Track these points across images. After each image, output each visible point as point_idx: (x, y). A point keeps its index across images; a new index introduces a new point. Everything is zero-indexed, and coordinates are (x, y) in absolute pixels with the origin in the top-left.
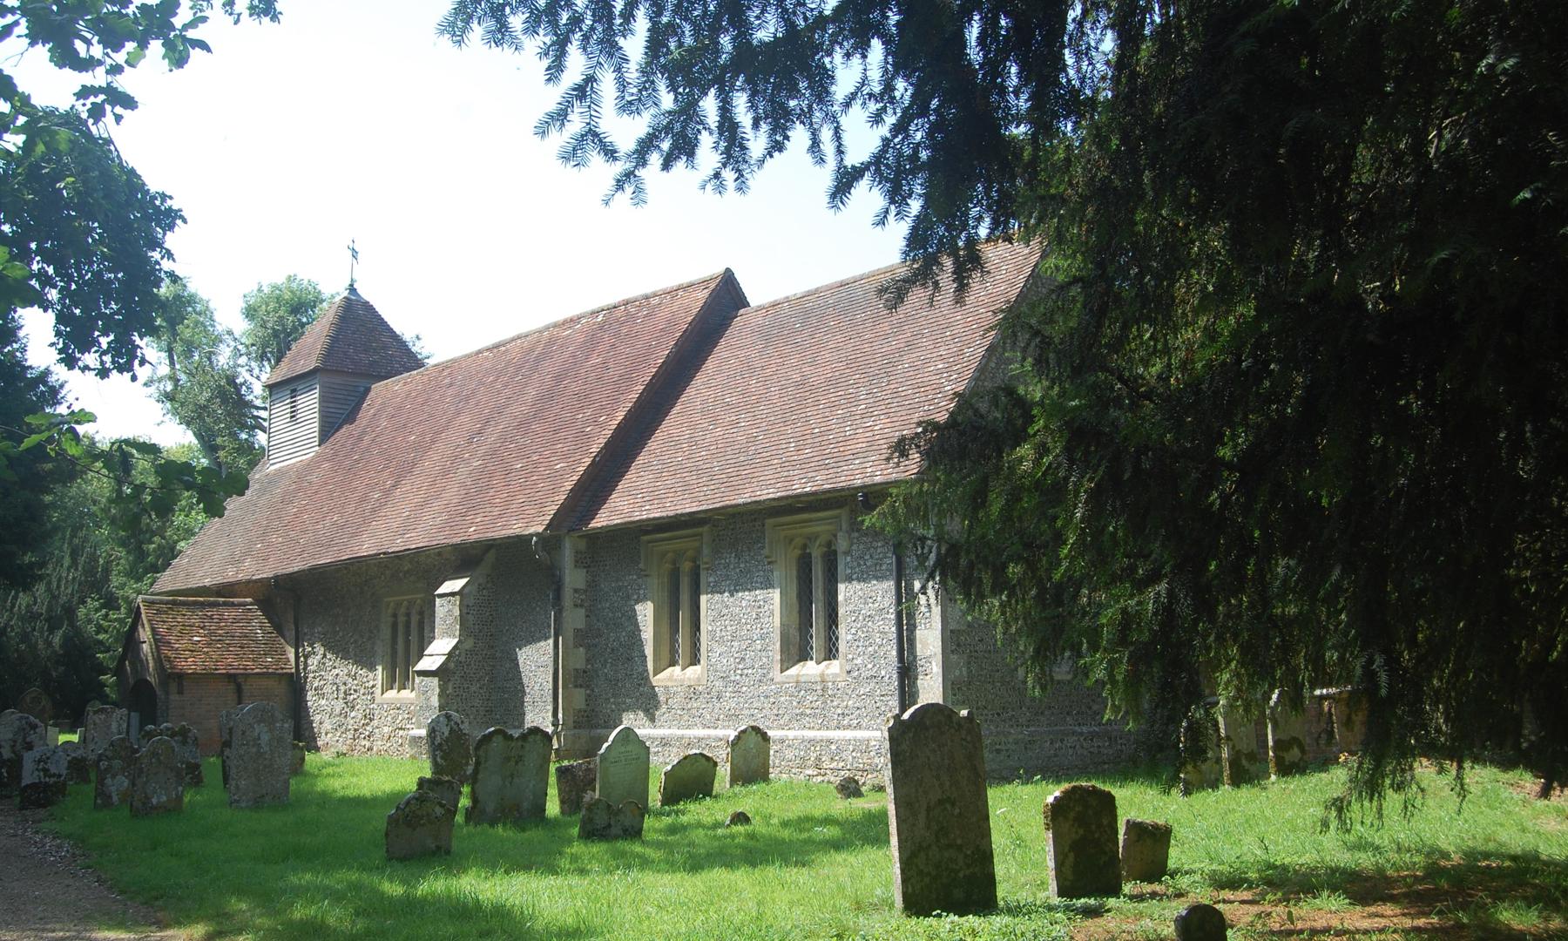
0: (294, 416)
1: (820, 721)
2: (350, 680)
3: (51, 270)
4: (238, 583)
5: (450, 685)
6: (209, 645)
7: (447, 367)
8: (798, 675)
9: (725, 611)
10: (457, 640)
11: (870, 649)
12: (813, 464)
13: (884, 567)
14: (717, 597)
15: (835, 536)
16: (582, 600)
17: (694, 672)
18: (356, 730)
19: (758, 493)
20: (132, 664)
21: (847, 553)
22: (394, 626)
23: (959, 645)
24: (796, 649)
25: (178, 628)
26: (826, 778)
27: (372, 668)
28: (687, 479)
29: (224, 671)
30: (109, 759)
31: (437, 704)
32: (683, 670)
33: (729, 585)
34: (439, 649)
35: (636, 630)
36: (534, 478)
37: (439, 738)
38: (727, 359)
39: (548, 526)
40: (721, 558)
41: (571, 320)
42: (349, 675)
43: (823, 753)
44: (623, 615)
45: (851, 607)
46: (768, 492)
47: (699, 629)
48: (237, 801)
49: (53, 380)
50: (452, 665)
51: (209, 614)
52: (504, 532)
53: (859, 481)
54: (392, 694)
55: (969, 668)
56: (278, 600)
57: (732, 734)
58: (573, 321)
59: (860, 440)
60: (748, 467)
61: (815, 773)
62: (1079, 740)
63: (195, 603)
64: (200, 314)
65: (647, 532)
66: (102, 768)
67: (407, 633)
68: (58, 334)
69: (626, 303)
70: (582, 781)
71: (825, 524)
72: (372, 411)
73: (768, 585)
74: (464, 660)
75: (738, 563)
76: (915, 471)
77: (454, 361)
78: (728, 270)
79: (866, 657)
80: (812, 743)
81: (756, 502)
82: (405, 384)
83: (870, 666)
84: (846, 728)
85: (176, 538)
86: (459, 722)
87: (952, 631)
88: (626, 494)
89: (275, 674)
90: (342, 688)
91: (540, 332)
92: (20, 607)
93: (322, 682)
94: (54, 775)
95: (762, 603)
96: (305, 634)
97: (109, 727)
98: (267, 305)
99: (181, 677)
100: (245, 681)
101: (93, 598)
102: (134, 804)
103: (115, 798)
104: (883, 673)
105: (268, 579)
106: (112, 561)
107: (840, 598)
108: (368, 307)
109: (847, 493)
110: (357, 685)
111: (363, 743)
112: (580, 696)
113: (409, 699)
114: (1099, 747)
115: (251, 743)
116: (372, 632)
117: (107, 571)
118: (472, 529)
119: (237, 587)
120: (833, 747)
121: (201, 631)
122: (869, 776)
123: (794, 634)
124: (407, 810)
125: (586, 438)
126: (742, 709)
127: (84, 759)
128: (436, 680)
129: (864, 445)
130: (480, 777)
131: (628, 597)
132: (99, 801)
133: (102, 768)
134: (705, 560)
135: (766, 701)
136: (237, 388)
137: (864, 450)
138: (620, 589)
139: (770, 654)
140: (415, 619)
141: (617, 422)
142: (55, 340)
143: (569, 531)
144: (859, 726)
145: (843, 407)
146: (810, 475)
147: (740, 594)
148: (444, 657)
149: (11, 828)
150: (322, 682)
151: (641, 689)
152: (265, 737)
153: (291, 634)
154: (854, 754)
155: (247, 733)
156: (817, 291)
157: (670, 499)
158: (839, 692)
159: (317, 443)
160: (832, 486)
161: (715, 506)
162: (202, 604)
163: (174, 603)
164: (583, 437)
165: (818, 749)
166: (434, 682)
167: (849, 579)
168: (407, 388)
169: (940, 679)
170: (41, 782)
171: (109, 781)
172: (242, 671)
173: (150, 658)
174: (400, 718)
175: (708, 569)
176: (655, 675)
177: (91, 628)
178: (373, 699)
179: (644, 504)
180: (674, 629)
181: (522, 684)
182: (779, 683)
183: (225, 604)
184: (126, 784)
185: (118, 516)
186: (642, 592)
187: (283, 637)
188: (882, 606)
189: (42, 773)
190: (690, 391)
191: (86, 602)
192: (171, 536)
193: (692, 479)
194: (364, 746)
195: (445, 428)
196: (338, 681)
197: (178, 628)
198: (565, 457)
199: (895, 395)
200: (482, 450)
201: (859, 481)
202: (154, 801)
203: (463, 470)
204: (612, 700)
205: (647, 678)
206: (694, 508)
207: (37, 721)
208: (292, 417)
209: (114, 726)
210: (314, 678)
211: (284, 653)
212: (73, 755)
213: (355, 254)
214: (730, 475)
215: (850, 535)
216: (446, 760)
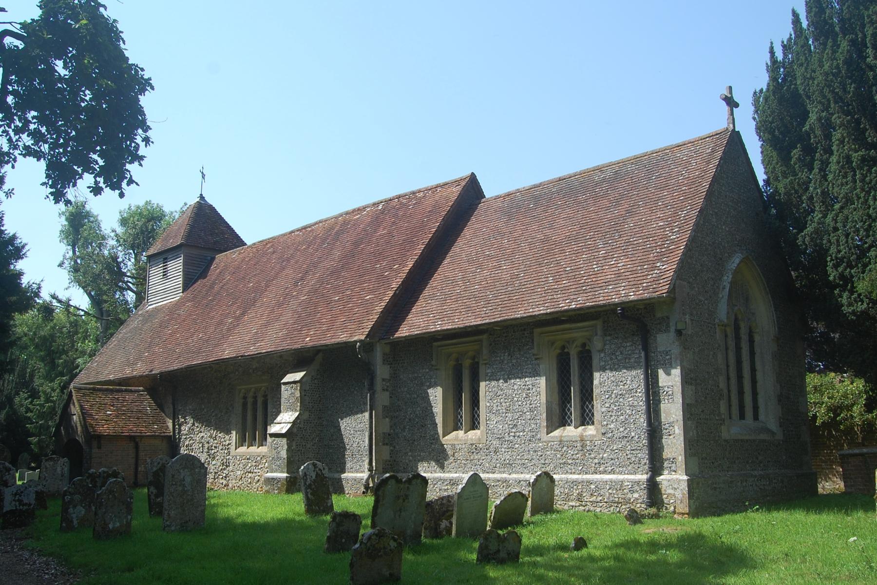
0: (166, 275)
1: (581, 468)
2: (212, 440)
3: (44, 130)
4: (134, 377)
5: (294, 444)
6: (117, 417)
8: (561, 436)
9: (500, 393)
10: (297, 414)
11: (622, 417)
12: (572, 290)
14: (493, 383)
15: (589, 340)
16: (388, 387)
18: (215, 473)
19: (531, 310)
20: (66, 429)
22: (245, 405)
23: (691, 415)
25: (97, 406)
27: (228, 432)
28: (467, 303)
29: (127, 434)
30: (71, 494)
31: (285, 456)
32: (465, 433)
35: (429, 406)
36: (351, 305)
37: (309, 480)
38: (480, 229)
39: (368, 336)
41: (359, 209)
42: (211, 437)
43: (584, 490)
46: (539, 309)
47: (256, 421)
48: (168, 526)
49: (18, 242)
50: (295, 430)
51: (117, 397)
52: (333, 340)
53: (617, 300)
54: (243, 449)
55: (697, 431)
56: (161, 388)
57: (532, 478)
58: (359, 210)
60: (517, 294)
61: (577, 504)
63: (107, 390)
64: (92, 222)
65: (437, 340)
66: (66, 501)
67: (255, 410)
68: (48, 176)
69: (399, 197)
70: (438, 513)
71: (587, 331)
72: (218, 271)
73: (535, 374)
76: (666, 291)
78: (473, 174)
79: (618, 423)
80: (575, 483)
81: (531, 316)
82: (240, 254)
83: (621, 429)
84: (605, 472)
85: (75, 356)
86: (322, 469)
87: (688, 404)
90: (206, 445)
91: (336, 217)
93: (191, 442)
94: (26, 504)
95: (530, 387)
96: (179, 410)
98: (134, 217)
99: (99, 437)
100: (141, 441)
101: (24, 392)
103: (75, 522)
104: (633, 434)
106: (35, 370)
107: (596, 382)
109: (608, 308)
110: (217, 443)
111: (221, 481)
112: (386, 450)
115: (179, 483)
116: (228, 409)
117: (32, 376)
118: (308, 339)
119: (130, 381)
120: (593, 487)
121: (112, 408)
122: (623, 507)
123: (556, 408)
124: (368, 544)
126: (515, 460)
128: (284, 440)
130: (379, 511)
131: (422, 384)
132: (64, 525)
133: (66, 501)
136: (118, 264)
137: (614, 279)
139: (538, 421)
140: (260, 400)
141: (409, 268)
143: (380, 339)
144: (613, 472)
145: (586, 253)
146: (572, 297)
147: (513, 381)
148: (289, 425)
150: (191, 442)
151: (433, 446)
152: (188, 479)
154: (610, 491)
155: (176, 477)
156: (540, 184)
157: (457, 317)
161: (496, 320)
162: (112, 391)
163: (94, 389)
164: (383, 281)
165: (580, 487)
167: (603, 369)
168: (241, 256)
169: (682, 438)
170: (16, 509)
171: (71, 510)
172: (139, 434)
173: (78, 425)
175: (486, 364)
176: (444, 436)
177: (23, 410)
178: (229, 452)
180: (458, 404)
181: (343, 443)
182: (545, 442)
183: (126, 391)
184: (83, 512)
185: (40, 343)
187: (164, 412)
189: (17, 503)
190: (455, 249)
191: (19, 394)
192: (72, 355)
193: (473, 303)
194: (222, 484)
197: (97, 406)
198: (371, 291)
199: (628, 244)
200: (307, 289)
202: (111, 526)
203: (294, 304)
205: (436, 439)
206: (479, 322)
207: (10, 466)
209: (59, 469)
210: (185, 438)
211: (165, 422)
213: (203, 176)
215: (603, 338)
216: (314, 496)
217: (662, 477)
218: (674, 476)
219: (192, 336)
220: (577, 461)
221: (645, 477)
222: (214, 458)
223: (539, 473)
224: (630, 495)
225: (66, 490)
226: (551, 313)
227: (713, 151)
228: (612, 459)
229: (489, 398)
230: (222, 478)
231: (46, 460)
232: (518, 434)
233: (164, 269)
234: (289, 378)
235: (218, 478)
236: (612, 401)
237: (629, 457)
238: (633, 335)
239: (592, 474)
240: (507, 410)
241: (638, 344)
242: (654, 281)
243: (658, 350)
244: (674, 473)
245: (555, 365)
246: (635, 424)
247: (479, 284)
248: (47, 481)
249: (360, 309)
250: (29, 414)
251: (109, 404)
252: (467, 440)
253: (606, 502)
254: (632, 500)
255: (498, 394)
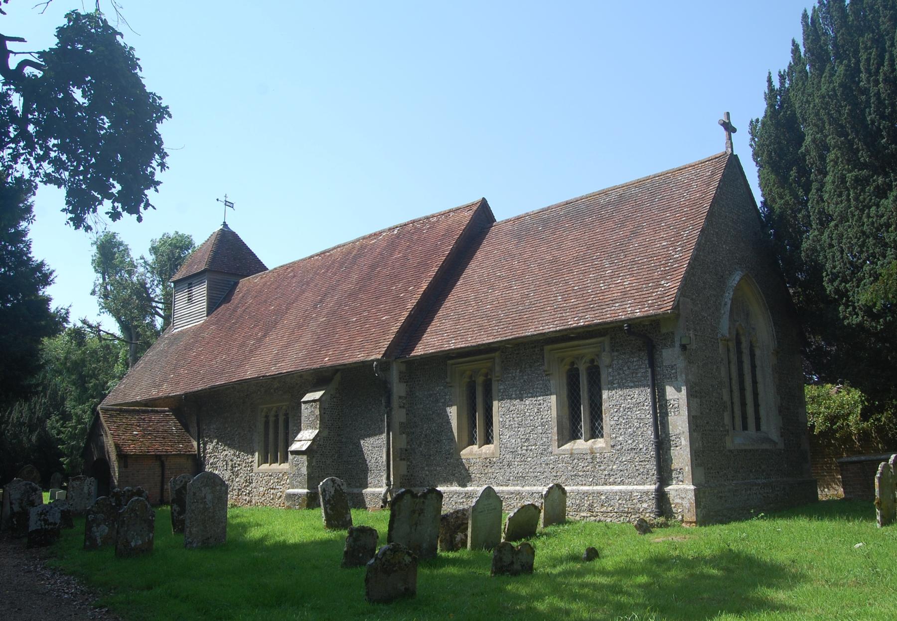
0: (190, 299)
1: (591, 480)
3: (64, 157)
4: (160, 398)
5: (314, 460)
6: (143, 437)
7: (290, 267)
10: (317, 431)
11: (630, 430)
12: (580, 308)
13: (639, 375)
16: (404, 404)
17: (487, 449)
18: (239, 490)
19: (541, 328)
21: (610, 366)
22: (267, 423)
23: (697, 426)
24: (568, 431)
26: (598, 518)
28: (480, 322)
29: (153, 453)
32: (479, 447)
33: (516, 391)
34: (305, 438)
36: (368, 326)
37: (328, 495)
39: (384, 355)
40: (509, 373)
41: (375, 234)
42: (234, 455)
43: (595, 501)
44: (433, 413)
45: (613, 403)
48: (191, 543)
50: (315, 447)
51: (143, 417)
52: (351, 360)
54: (265, 466)
59: (615, 292)
60: (527, 313)
61: (589, 515)
62: (758, 489)
63: (134, 411)
65: (453, 358)
68: (68, 203)
69: (413, 222)
73: (546, 392)
74: (322, 444)
75: (522, 376)
77: (294, 263)
78: (484, 199)
79: (626, 436)
80: (586, 495)
82: (261, 278)
83: (630, 442)
84: (614, 483)
86: (340, 484)
87: (693, 417)
88: (434, 334)
89: (184, 454)
91: (354, 242)
92: (13, 419)
93: (216, 460)
94: (51, 524)
95: (542, 402)
97: (82, 490)
101: (55, 414)
102: (118, 546)
103: (99, 541)
104: (641, 446)
105: (180, 395)
108: (235, 236)
110: (240, 461)
112: (403, 465)
113: (278, 469)
114: (767, 493)
115: (200, 501)
117: (63, 399)
118: (327, 359)
120: (603, 497)
122: (633, 516)
123: (566, 423)
124: (384, 560)
125: (401, 302)
126: (528, 473)
127: (69, 511)
128: (305, 457)
129: (619, 294)
132: (88, 543)
133: (90, 520)
134: (497, 375)
135: (547, 467)
137: (620, 297)
138: (431, 395)
139: (549, 435)
141: (423, 290)
142: (66, 207)
143: (396, 358)
144: (622, 483)
146: (580, 315)
148: (310, 443)
149: (25, 565)
150: (216, 460)
151: (448, 461)
152: (209, 497)
153: (194, 429)
154: (620, 502)
155: (197, 494)
156: (548, 208)
158: (605, 460)
159: (205, 315)
160: (601, 321)
161: (507, 338)
162: (138, 411)
163: (121, 410)
164: (399, 302)
166: (304, 458)
168: (263, 280)
169: (688, 449)
171: (94, 529)
172: (165, 453)
174: (272, 482)
175: (498, 381)
179: (450, 339)
183: (152, 411)
184: (106, 531)
186: (447, 397)
188: (638, 401)
189: (43, 522)
190: (468, 271)
193: (485, 322)
194: (246, 500)
195: (296, 300)
196: (227, 459)
198: (387, 312)
199: (634, 263)
200: (325, 311)
201: (623, 317)
202: (133, 544)
203: (313, 325)
204: (426, 468)
207: (37, 486)
208: (189, 300)
210: (210, 457)
211: (190, 442)
212: (62, 509)
214: (514, 318)
217: (670, 487)
218: (682, 486)
219: (215, 358)
220: (588, 473)
221: (653, 487)
222: (237, 475)
223: (551, 485)
224: (639, 505)
225: (89, 510)
226: (560, 331)
227: (713, 174)
228: (621, 471)
229: (502, 413)
230: (246, 495)
231: (73, 480)
232: (530, 448)
233: (189, 294)
234: (309, 397)
235: (241, 494)
236: (620, 415)
237: (637, 468)
238: (639, 350)
239: (602, 485)
240: (520, 426)
241: (644, 358)
242: (659, 298)
243: (664, 364)
244: (681, 483)
245: (565, 381)
246: (642, 436)
247: (491, 303)
248: (74, 500)
249: (377, 329)
250: (62, 436)
251: (135, 424)
252: (481, 454)
253: (616, 512)
254: (641, 510)
255: (510, 410)
